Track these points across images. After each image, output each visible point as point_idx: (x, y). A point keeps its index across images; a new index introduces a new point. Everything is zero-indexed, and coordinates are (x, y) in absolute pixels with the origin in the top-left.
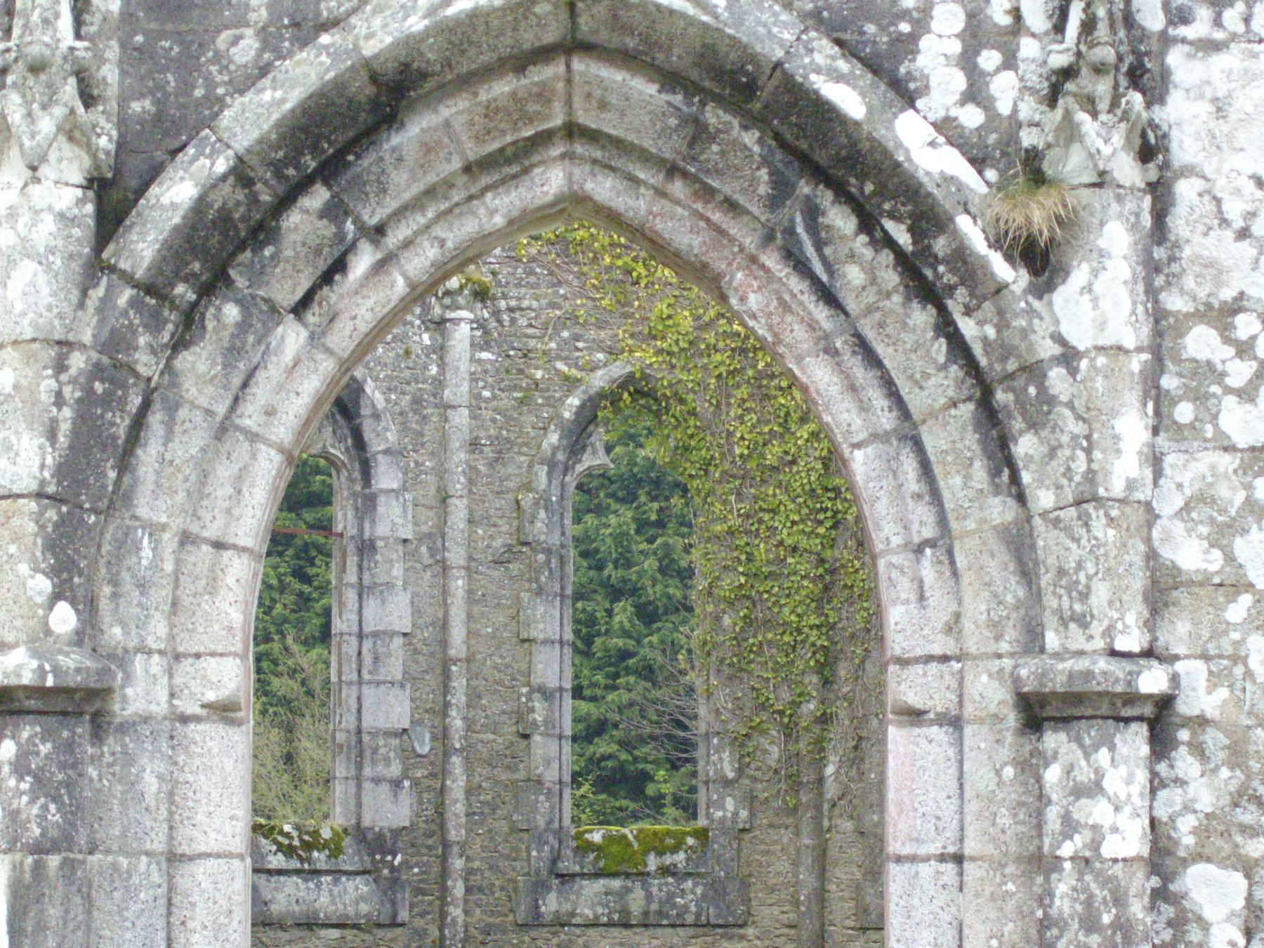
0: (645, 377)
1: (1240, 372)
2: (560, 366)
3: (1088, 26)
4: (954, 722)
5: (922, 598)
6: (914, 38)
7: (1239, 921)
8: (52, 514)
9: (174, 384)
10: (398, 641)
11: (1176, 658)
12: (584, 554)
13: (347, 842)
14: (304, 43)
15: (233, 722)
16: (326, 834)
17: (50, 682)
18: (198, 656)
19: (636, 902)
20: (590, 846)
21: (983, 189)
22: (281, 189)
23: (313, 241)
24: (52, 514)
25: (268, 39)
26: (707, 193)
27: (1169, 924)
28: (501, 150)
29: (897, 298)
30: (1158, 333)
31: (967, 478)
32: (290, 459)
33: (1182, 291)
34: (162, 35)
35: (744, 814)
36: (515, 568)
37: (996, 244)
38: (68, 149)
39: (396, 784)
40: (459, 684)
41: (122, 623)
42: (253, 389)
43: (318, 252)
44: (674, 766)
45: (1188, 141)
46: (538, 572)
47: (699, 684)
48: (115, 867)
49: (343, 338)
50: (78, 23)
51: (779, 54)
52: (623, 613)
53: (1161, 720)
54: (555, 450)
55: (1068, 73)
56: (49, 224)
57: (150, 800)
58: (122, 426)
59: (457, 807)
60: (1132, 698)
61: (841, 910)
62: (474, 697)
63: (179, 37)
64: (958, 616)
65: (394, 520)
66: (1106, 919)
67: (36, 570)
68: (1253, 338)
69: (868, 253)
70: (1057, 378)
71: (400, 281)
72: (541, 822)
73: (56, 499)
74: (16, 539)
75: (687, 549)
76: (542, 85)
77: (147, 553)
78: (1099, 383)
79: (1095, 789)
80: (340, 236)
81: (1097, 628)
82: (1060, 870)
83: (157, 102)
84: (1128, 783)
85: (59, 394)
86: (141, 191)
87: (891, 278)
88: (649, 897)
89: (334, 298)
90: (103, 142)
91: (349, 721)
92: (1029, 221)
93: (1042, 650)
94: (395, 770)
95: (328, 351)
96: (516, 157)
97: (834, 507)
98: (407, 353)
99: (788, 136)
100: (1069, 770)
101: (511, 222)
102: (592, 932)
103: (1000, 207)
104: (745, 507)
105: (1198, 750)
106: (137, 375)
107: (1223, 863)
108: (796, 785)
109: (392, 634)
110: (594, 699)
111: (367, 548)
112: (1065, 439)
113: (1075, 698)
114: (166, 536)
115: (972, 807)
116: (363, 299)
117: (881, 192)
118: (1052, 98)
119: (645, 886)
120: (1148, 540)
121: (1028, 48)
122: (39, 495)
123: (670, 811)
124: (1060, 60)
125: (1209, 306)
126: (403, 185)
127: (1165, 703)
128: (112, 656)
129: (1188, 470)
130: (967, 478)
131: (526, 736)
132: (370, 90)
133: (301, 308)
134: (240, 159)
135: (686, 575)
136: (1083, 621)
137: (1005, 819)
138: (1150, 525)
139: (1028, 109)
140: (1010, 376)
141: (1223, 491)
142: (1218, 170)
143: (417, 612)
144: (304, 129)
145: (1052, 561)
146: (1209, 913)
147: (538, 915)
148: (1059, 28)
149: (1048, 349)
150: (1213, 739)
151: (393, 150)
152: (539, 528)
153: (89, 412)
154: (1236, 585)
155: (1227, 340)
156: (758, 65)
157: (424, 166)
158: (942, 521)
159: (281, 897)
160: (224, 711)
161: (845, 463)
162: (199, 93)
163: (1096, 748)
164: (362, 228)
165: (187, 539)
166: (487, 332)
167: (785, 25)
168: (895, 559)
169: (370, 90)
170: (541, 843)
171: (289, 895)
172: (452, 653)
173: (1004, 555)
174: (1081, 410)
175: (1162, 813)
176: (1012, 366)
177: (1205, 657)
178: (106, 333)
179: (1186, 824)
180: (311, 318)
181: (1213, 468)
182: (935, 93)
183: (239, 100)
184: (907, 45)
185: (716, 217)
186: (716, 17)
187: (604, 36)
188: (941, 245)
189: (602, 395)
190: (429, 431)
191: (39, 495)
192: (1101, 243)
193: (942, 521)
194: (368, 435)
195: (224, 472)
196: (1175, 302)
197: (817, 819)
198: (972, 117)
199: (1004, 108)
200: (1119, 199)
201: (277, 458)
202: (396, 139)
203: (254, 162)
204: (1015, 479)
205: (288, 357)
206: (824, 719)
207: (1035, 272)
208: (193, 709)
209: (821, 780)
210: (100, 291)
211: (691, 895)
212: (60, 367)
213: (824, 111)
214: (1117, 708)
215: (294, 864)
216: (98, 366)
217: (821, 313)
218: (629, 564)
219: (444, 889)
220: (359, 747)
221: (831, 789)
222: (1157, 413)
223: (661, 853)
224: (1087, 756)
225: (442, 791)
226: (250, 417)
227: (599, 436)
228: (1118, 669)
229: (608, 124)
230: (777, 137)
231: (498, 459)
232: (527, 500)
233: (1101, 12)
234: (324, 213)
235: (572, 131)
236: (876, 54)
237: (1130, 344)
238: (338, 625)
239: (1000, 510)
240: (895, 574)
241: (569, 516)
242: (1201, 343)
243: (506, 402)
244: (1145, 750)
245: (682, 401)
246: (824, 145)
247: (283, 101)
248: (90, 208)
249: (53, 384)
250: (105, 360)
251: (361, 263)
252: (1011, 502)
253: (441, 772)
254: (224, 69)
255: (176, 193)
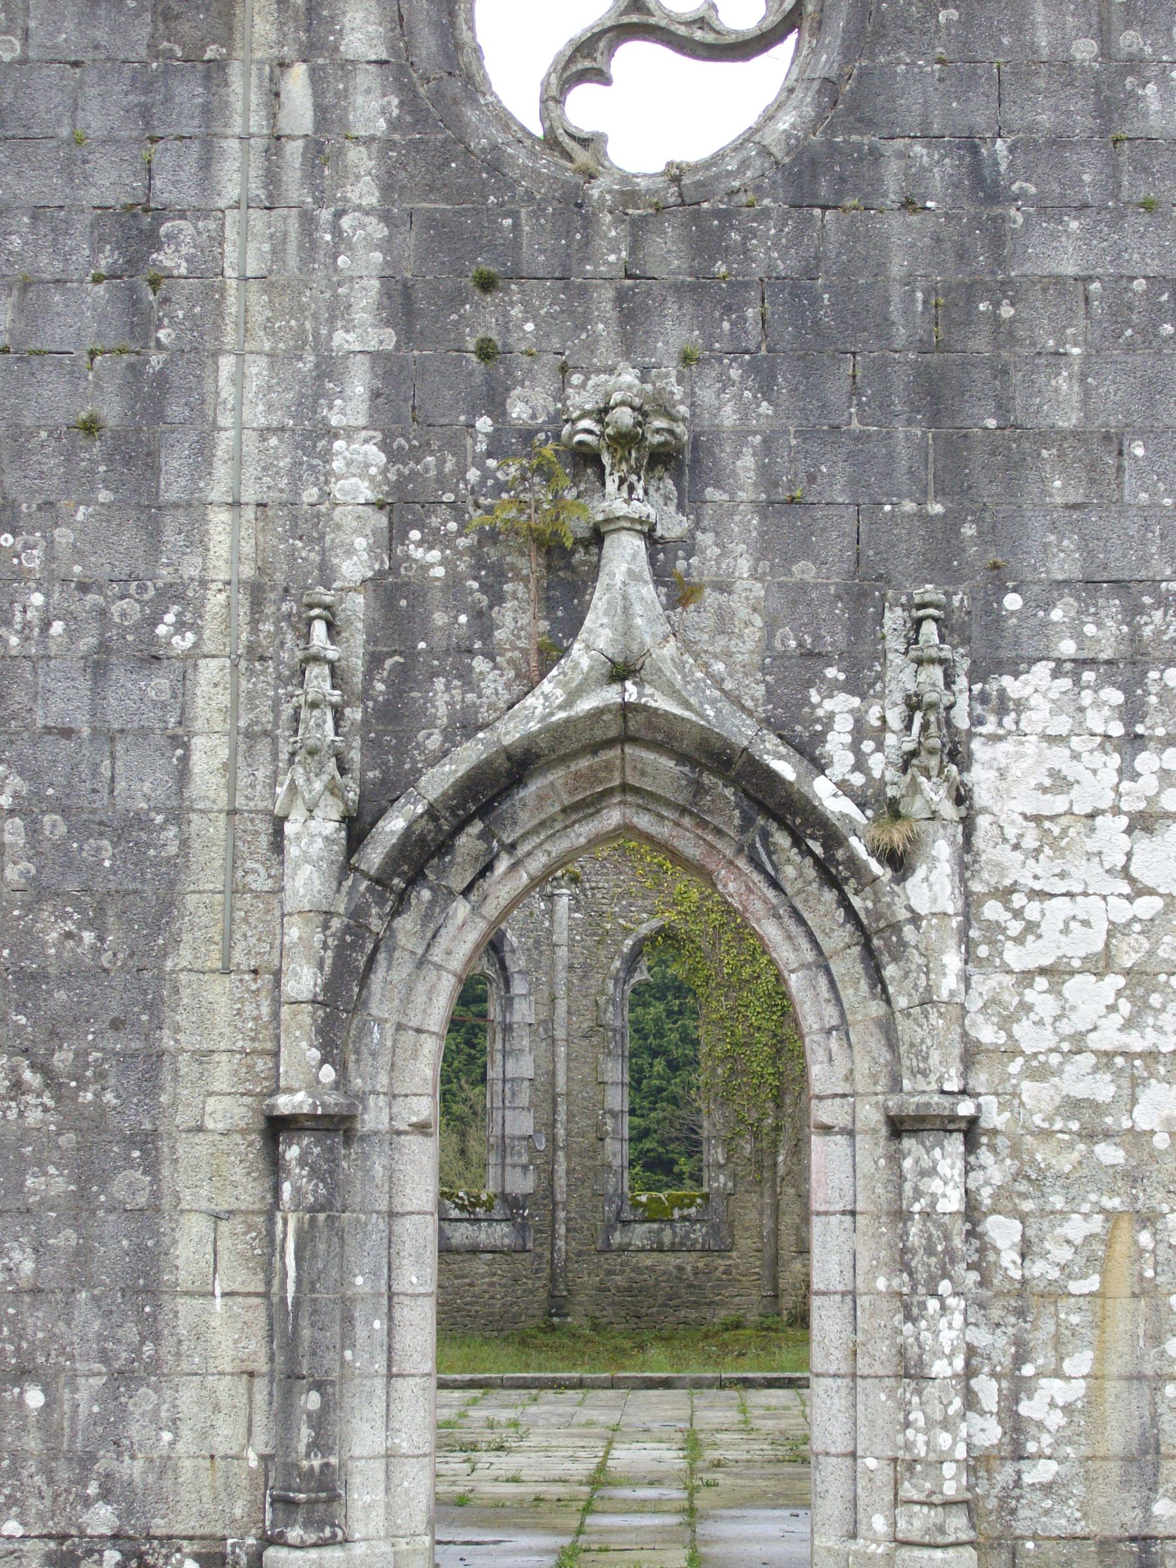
0: (671, 927)
1: (1015, 928)
2: (621, 921)
3: (925, 727)
4: (850, 1133)
5: (831, 1060)
6: (824, 733)
7: (1018, 1249)
8: (321, 1013)
9: (393, 936)
10: (526, 1084)
11: (980, 1094)
12: (636, 1031)
13: (496, 1202)
14: (468, 737)
15: (427, 1135)
16: (484, 1197)
17: (319, 1111)
18: (406, 1096)
19: (667, 1237)
20: (640, 1204)
21: (865, 821)
22: (455, 822)
23: (474, 853)
24: (321, 1013)
25: (448, 735)
26: (703, 824)
27: (977, 1251)
28: (584, 799)
29: (815, 885)
30: (967, 905)
31: (857, 989)
32: (460, 980)
33: (981, 881)
34: (386, 733)
35: (730, 1184)
36: (595, 1040)
37: (871, 853)
38: (331, 800)
39: (525, 1168)
40: (562, 1109)
41: (361, 1076)
42: (438, 939)
43: (477, 859)
44: (690, 1155)
45: (983, 793)
46: (609, 1042)
47: (703, 1107)
48: (358, 1220)
49: (491, 909)
50: (337, 726)
51: (746, 743)
52: (659, 1065)
53: (971, 1131)
54: (618, 970)
55: (914, 754)
56: (319, 843)
57: (378, 1180)
58: (362, 961)
59: (561, 1182)
60: (954, 1118)
61: (788, 1241)
62: (570, 1116)
63: (395, 734)
64: (852, 1071)
65: (523, 1012)
66: (940, 1248)
67: (311, 1046)
68: (1023, 907)
69: (798, 859)
70: (908, 931)
71: (525, 876)
72: (611, 1190)
73: (323, 1004)
74: (300, 1027)
75: (696, 1028)
76: (607, 761)
77: (376, 1035)
78: (933, 935)
79: (932, 1172)
80: (490, 849)
81: (933, 1078)
82: (913, 1219)
83: (383, 772)
84: (952, 1168)
85: (325, 942)
86: (373, 824)
87: (811, 873)
88: (675, 1234)
89: (486, 886)
90: (351, 795)
91: (497, 1131)
92: (891, 840)
93: (901, 1090)
94: (525, 1159)
95: (484, 917)
96: (592, 804)
97: (781, 1003)
98: (531, 914)
99: (752, 792)
100: (917, 1161)
101: (589, 841)
102: (641, 1255)
103: (874, 832)
104: (730, 1003)
105: (993, 1148)
106: (371, 932)
107: (1007, 1215)
108: (760, 1167)
109: (522, 1079)
110: (642, 1116)
111: (507, 1028)
112: (913, 967)
113: (921, 1119)
114: (388, 1025)
115: (861, 1183)
116: (503, 886)
117: (806, 823)
118: (904, 770)
119: (673, 1228)
120: (962, 1026)
121: (890, 739)
122: (314, 1002)
123: (688, 1182)
124: (909, 746)
125: (997, 889)
126: (527, 819)
127: (973, 1121)
128: (356, 1096)
129: (986, 985)
130: (857, 989)
131: (602, 1139)
132: (507, 765)
133: (466, 892)
134: (431, 805)
135: (696, 1043)
136: (925, 1073)
137: (880, 1190)
138: (963, 1017)
139: (891, 774)
140: (882, 930)
141: (1006, 997)
142: (1001, 810)
143: (537, 1067)
144: (469, 788)
145: (906, 1038)
146: (999, 1244)
147: (609, 1245)
148: (908, 728)
149: (903, 914)
150: (1001, 1142)
151: (521, 799)
152: (609, 1016)
153: (342, 953)
154: (1014, 1052)
155: (1007, 909)
156: (732, 749)
157: (539, 808)
158: (842, 1015)
159: (457, 1235)
160: (421, 1128)
161: (785, 981)
162: (407, 766)
163: (933, 1148)
164: (502, 845)
165: (400, 1027)
166: (578, 901)
167: (748, 726)
168: (815, 1038)
169: (507, 765)
170: (611, 1202)
171: (461, 1234)
172: (558, 1090)
173: (879, 1036)
174: (923, 950)
175: (972, 1186)
176: (882, 924)
177: (997, 1094)
178: (353, 906)
179: (986, 1192)
180: (473, 897)
181: (1000, 983)
182: (836, 766)
183: (431, 771)
184: (820, 738)
185: (709, 838)
186: (709, 722)
187: (643, 733)
188: (840, 854)
189: (645, 938)
190: (545, 961)
191: (314, 1002)
192: (934, 853)
193: (842, 1015)
194: (508, 962)
195: (421, 988)
196: (977, 887)
197: (774, 1187)
198: (858, 779)
199: (877, 774)
200: (944, 827)
201: (453, 980)
202: (522, 793)
203: (439, 806)
204: (884, 990)
205: (459, 920)
206: (777, 1129)
207: (895, 870)
208: (404, 1127)
209: (775, 1164)
210: (350, 882)
211: (699, 1233)
212: (326, 927)
213: (773, 777)
214: (946, 1124)
215: (466, 1215)
216: (348, 927)
217: (771, 894)
218: (662, 1036)
219: (554, 1230)
220: (503, 1147)
221: (782, 1170)
222: (967, 951)
223: (681, 1208)
224: (928, 1153)
225: (553, 1172)
226: (437, 955)
227: (644, 962)
228: (946, 1101)
229: (647, 785)
230: (744, 791)
231: (585, 976)
232: (602, 1000)
233: (932, 719)
234: (481, 836)
235: (625, 788)
236: (801, 743)
237: (951, 911)
238: (491, 1074)
239: (876, 1009)
240: (815, 1047)
241: (626, 1009)
242: (992, 910)
243: (589, 942)
244: (962, 1149)
245: (693, 942)
246: (772, 796)
247: (456, 771)
248: (343, 834)
249: (322, 936)
250: (352, 922)
251: (502, 865)
252: (882, 1004)
253: (553, 1161)
254: (422, 753)
255: (395, 824)
